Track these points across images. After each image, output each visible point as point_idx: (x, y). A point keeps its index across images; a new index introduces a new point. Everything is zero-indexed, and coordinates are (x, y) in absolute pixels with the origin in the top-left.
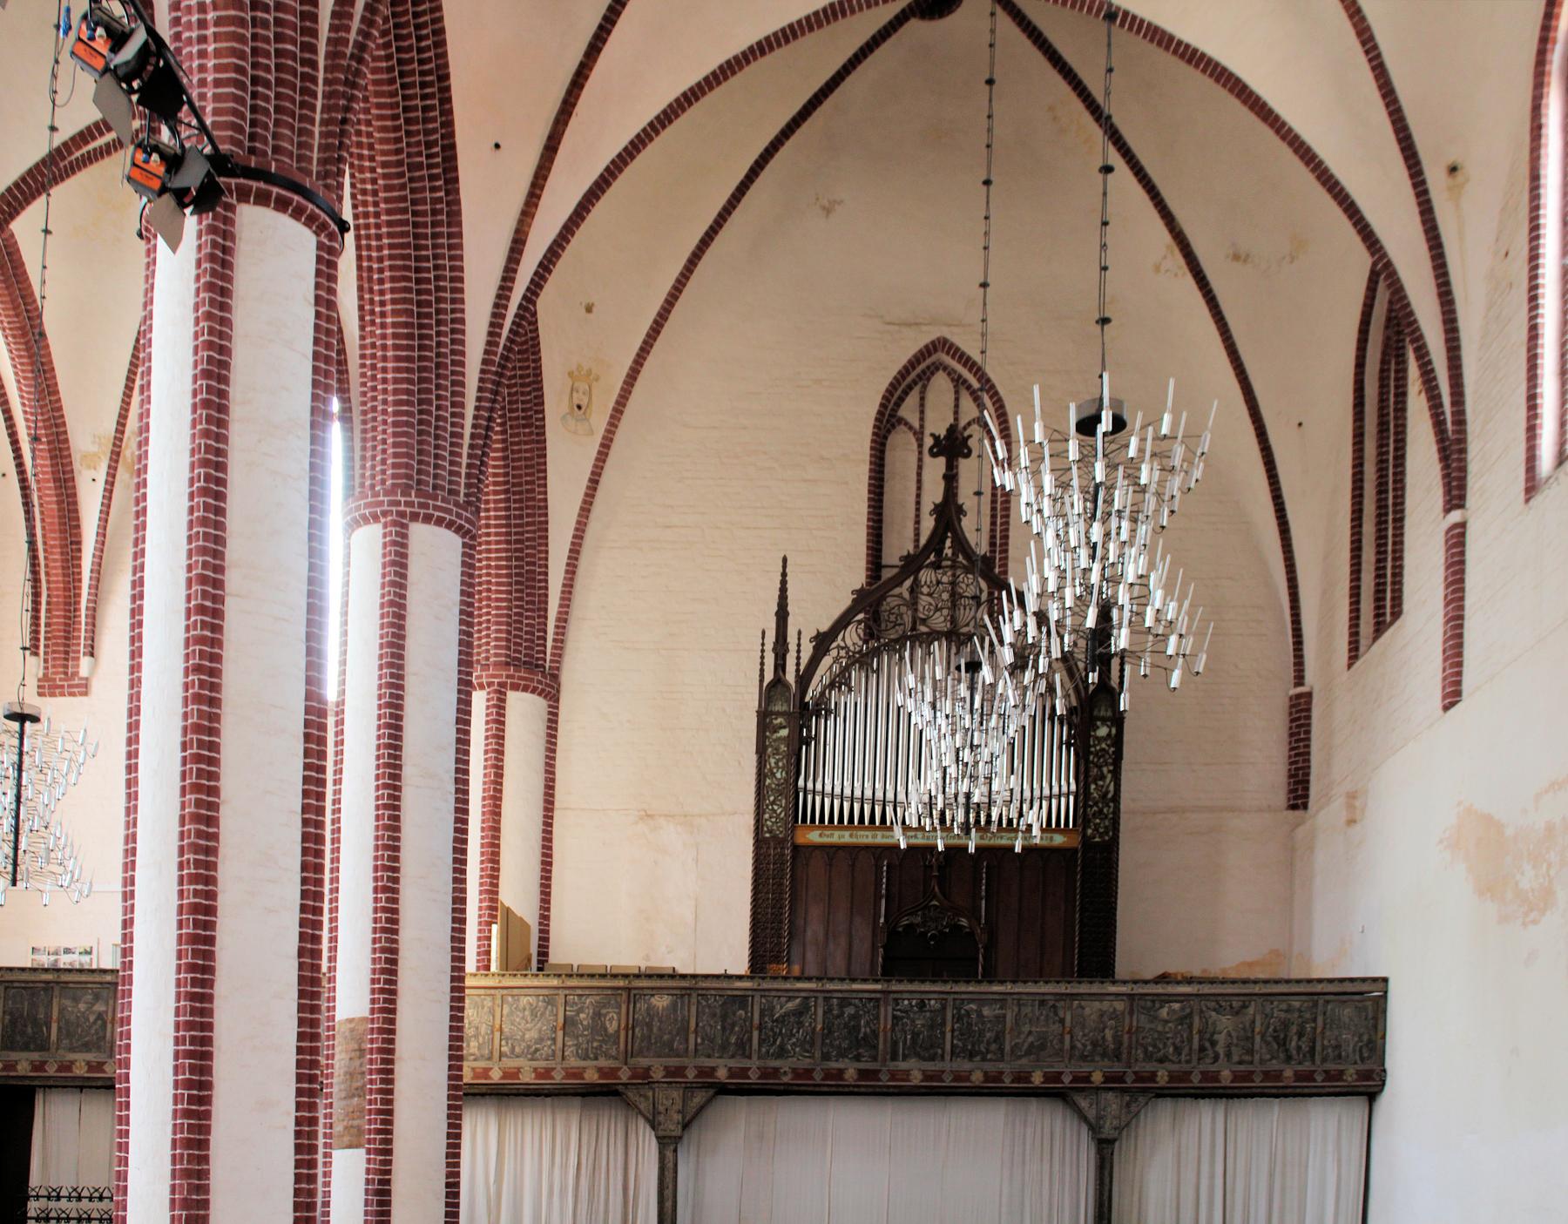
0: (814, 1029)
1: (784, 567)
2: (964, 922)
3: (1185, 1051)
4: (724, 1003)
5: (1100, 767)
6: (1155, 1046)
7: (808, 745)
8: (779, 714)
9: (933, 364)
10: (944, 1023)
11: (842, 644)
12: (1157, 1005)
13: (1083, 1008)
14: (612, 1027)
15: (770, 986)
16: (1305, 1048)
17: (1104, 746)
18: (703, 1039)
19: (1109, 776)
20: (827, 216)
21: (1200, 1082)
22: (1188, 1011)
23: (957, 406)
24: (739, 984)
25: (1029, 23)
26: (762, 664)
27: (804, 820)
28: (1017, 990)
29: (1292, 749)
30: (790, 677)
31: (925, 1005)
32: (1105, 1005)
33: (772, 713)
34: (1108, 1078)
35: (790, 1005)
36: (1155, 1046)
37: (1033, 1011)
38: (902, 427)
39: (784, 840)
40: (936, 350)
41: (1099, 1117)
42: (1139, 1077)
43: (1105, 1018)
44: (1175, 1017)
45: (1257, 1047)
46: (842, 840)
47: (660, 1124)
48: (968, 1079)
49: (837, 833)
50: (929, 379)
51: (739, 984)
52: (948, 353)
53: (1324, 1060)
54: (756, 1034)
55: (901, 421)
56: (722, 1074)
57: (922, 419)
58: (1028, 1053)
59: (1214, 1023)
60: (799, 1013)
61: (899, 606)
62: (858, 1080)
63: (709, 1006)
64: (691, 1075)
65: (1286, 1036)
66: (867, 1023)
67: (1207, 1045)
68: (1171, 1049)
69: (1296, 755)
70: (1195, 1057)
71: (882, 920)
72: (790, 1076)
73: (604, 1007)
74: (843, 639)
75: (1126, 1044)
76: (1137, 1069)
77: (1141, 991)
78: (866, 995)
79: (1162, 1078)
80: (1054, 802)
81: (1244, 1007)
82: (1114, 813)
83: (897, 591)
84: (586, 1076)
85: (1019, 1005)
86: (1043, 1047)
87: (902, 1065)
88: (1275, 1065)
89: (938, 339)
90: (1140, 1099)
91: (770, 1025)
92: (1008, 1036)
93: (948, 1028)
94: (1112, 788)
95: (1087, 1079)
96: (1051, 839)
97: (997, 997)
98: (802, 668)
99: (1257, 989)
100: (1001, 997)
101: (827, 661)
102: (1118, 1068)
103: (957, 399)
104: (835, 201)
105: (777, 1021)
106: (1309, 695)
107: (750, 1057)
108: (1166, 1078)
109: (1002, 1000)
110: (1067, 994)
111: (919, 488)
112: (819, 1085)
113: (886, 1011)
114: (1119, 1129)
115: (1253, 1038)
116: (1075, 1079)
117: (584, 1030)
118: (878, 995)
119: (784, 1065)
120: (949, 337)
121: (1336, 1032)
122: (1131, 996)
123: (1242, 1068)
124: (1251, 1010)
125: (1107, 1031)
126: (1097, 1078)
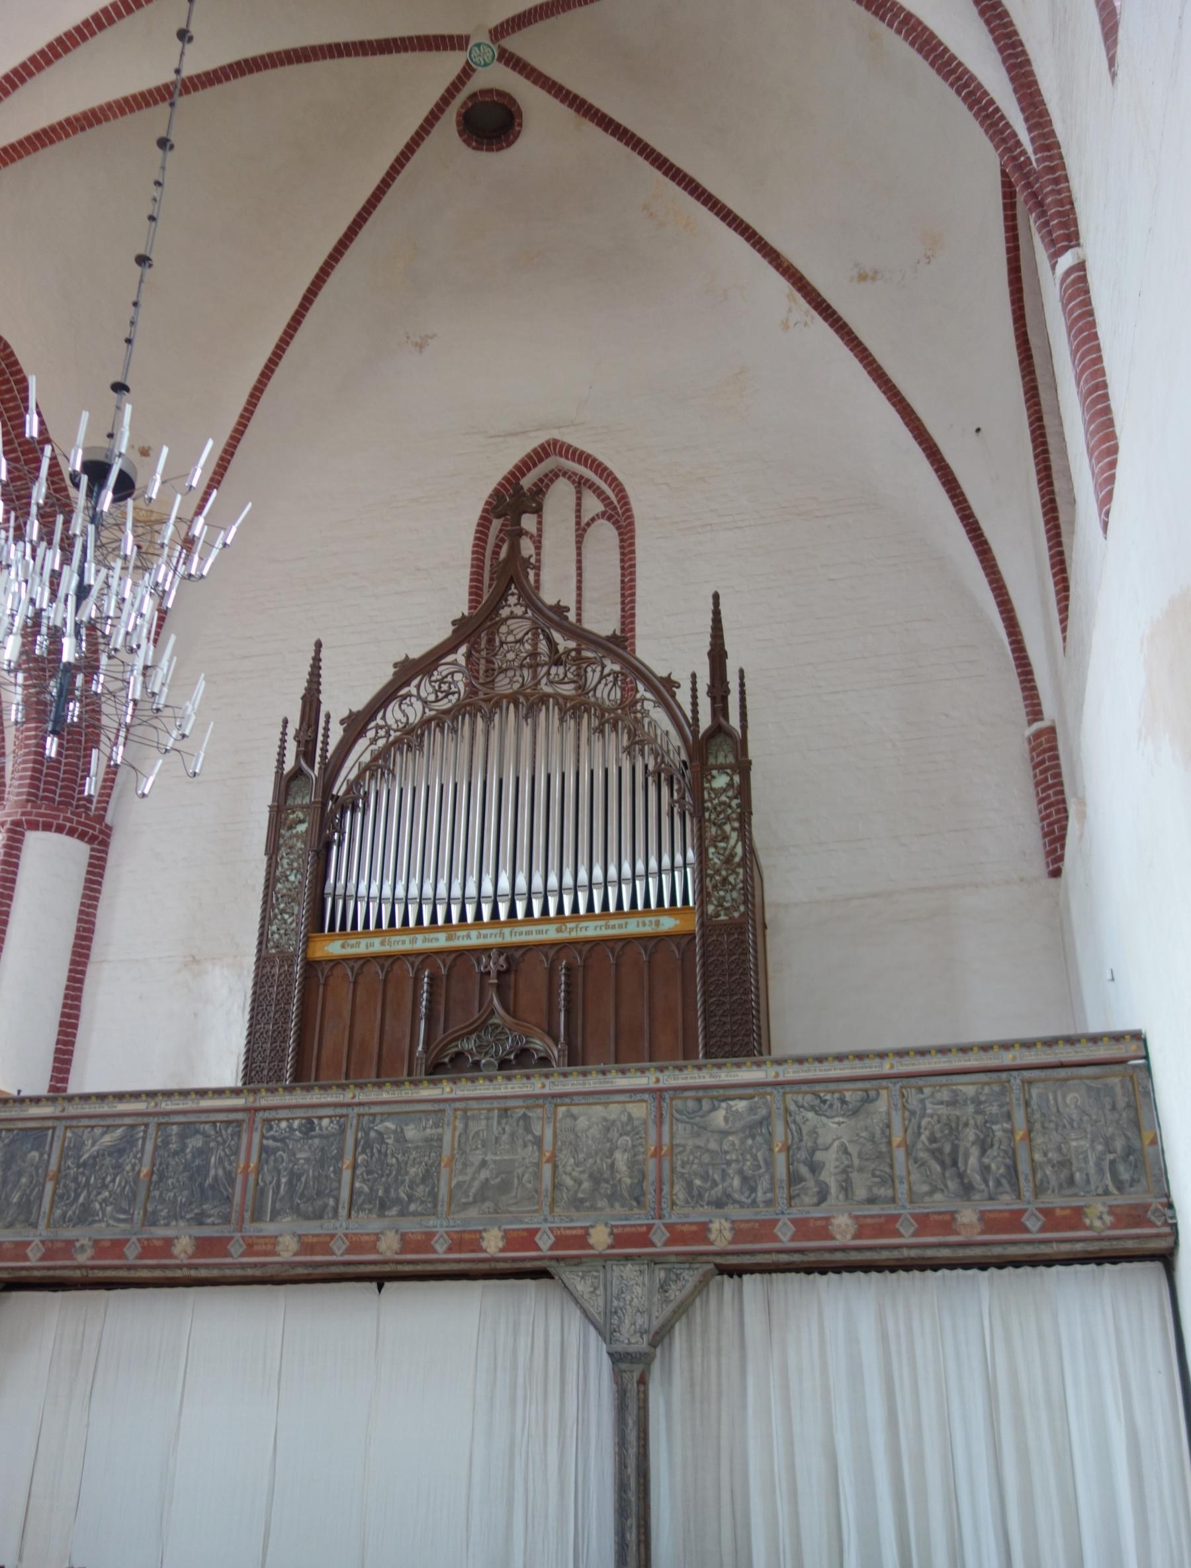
3: (763, 1184)
4: (13, 1141)
5: (720, 826)
6: (705, 1177)
10: (340, 1157)
11: (381, 723)
12: (706, 1105)
13: (575, 1118)
16: (997, 1167)
17: (723, 798)
19: (734, 835)
20: (421, 352)
21: (793, 1239)
22: (763, 1112)
24: (35, 1111)
25: (568, 92)
26: (282, 748)
28: (460, 1094)
29: (1041, 801)
31: (313, 1129)
32: (614, 1111)
34: (620, 1239)
35: (107, 1139)
36: (705, 1177)
40: (548, 455)
42: (676, 1235)
43: (614, 1134)
44: (739, 1125)
45: (900, 1170)
48: (374, 1249)
49: (363, 942)
51: (35, 1111)
53: (1038, 1190)
54: (49, 1186)
58: (481, 1197)
59: (814, 1132)
60: (118, 1151)
61: (452, 674)
65: (955, 1149)
67: (804, 1170)
68: (736, 1182)
69: (1046, 808)
70: (782, 1194)
71: (420, 1048)
72: (90, 1252)
74: (384, 718)
75: (652, 1176)
76: (674, 1219)
77: (673, 1083)
81: (867, 1100)
82: (744, 881)
85: (466, 1119)
86: (505, 1187)
87: (269, 1228)
88: (939, 1203)
89: (548, 442)
90: (686, 1274)
91: (72, 1172)
92: (444, 1172)
93: (348, 1161)
94: (739, 850)
95: (582, 1240)
96: (658, 923)
99: (886, 1067)
100: (437, 1107)
101: (362, 743)
102: (638, 1219)
103: (579, 499)
104: (427, 336)
105: (84, 1164)
106: (1052, 730)
107: (35, 1225)
108: (728, 1235)
109: (437, 1110)
110: (545, 1096)
115: (890, 1152)
118: (239, 1116)
120: (558, 437)
121: (1056, 1137)
122: (658, 1093)
123: (875, 1210)
124: (882, 1105)
126: (600, 1238)
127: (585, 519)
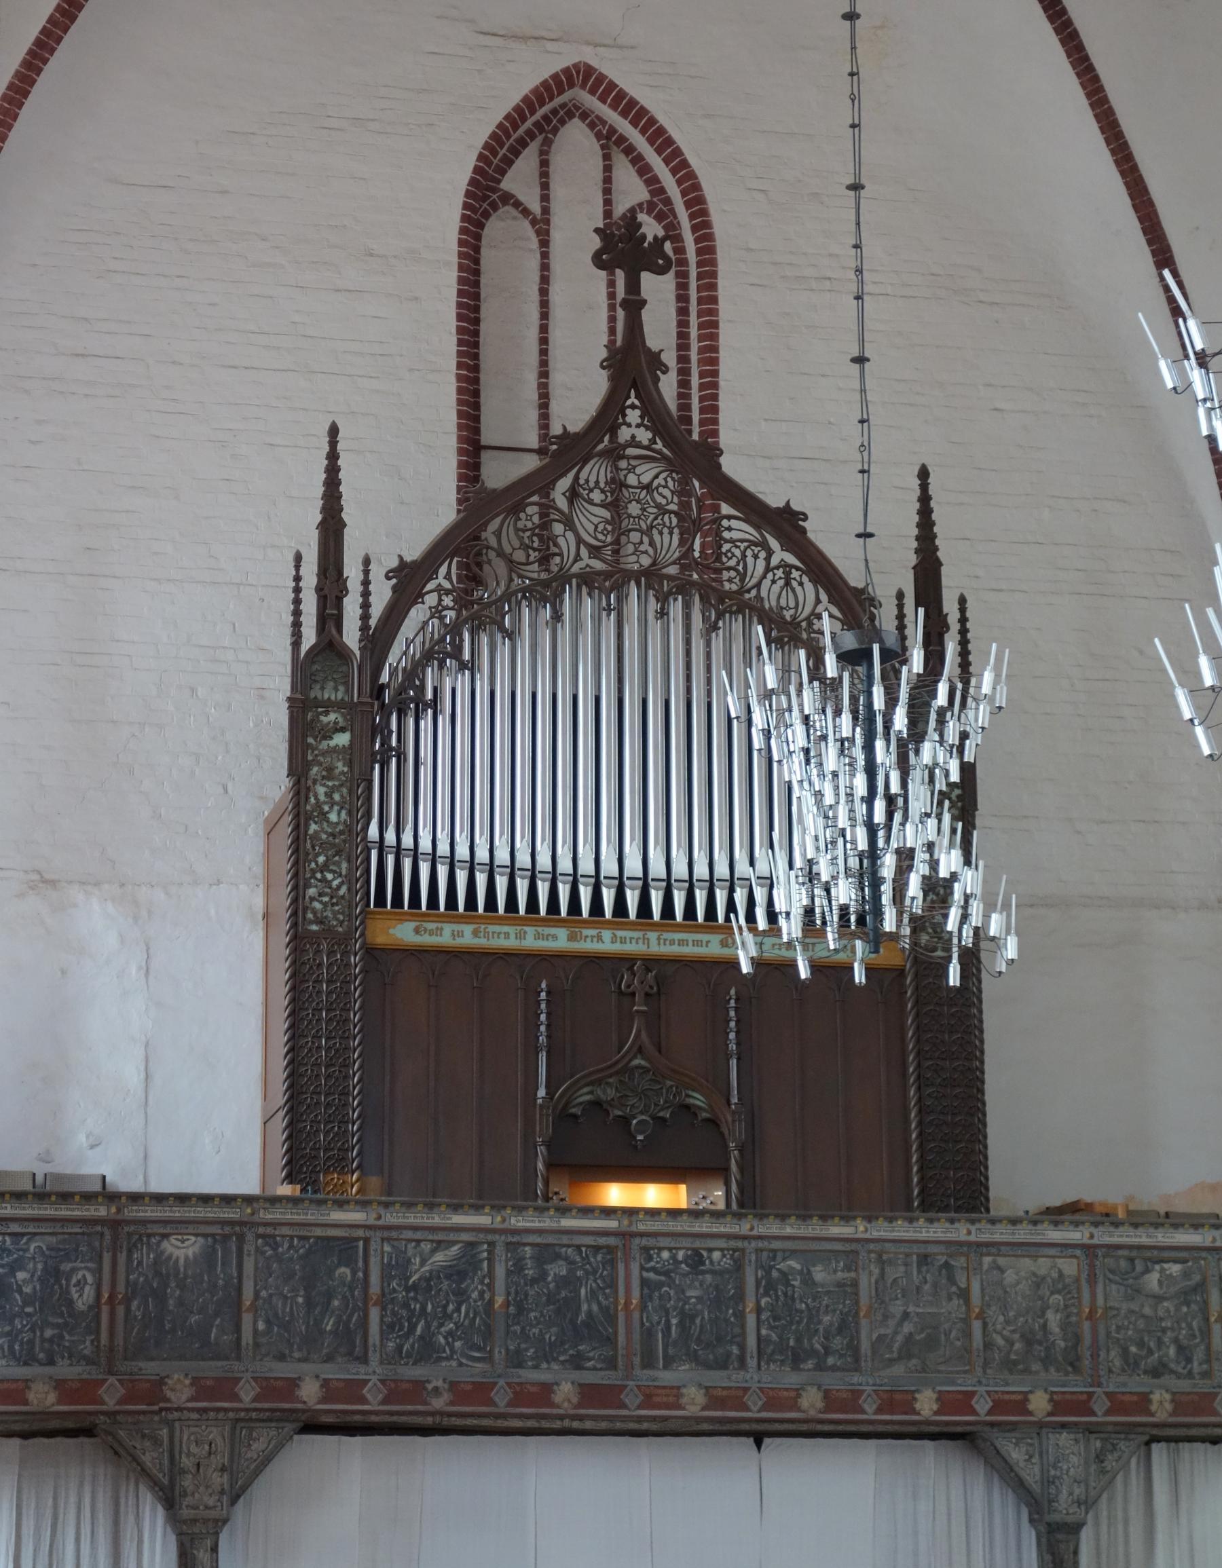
0: (491, 1302)
1: (333, 443)
2: (698, 1099)
3: (1199, 1354)
6: (1141, 1344)
7: (384, 765)
8: (329, 706)
9: (563, 106)
10: (740, 1297)
12: (1139, 1267)
13: (1001, 1270)
14: (83, 1299)
15: (400, 1221)
18: (268, 1322)
22: (1197, 1278)
23: (607, 180)
26: (297, 613)
27: (381, 900)
28: (875, 1234)
30: (351, 636)
32: (1042, 1266)
33: (317, 703)
34: (1060, 1405)
35: (440, 1258)
37: (908, 1274)
38: (509, 209)
39: (347, 938)
40: (571, 85)
41: (1048, 1482)
42: (1117, 1405)
44: (1173, 1290)
46: (460, 942)
47: (184, 1494)
48: (795, 1407)
49: (448, 928)
50: (555, 131)
52: (592, 92)
55: (508, 198)
56: (309, 1392)
57: (545, 198)
58: (907, 1351)
60: (459, 1273)
62: (579, 1405)
63: (279, 1258)
64: (247, 1394)
66: (593, 1294)
68: (1172, 1351)
71: (542, 1093)
73: (67, 1257)
76: (1111, 1389)
77: (1107, 1240)
78: (589, 1240)
79: (1161, 1404)
84: (31, 1396)
85: (881, 1261)
86: (932, 1343)
87: (666, 1377)
90: (1122, 1445)
91: (401, 1295)
92: (864, 1322)
93: (750, 1305)
95: (1021, 1406)
97: (838, 1246)
98: (373, 622)
101: (417, 615)
102: (1076, 1386)
103: (608, 169)
105: (415, 1287)
107: (364, 1360)
108: (1169, 1406)
109: (850, 1253)
110: (969, 1244)
111: (545, 316)
112: (504, 1416)
113: (627, 1268)
114: (1088, 1503)
116: (998, 1406)
117: (26, 1303)
119: (435, 1375)
120: (594, 63)
122: (1089, 1250)
125: (1050, 1315)
126: (1039, 1403)
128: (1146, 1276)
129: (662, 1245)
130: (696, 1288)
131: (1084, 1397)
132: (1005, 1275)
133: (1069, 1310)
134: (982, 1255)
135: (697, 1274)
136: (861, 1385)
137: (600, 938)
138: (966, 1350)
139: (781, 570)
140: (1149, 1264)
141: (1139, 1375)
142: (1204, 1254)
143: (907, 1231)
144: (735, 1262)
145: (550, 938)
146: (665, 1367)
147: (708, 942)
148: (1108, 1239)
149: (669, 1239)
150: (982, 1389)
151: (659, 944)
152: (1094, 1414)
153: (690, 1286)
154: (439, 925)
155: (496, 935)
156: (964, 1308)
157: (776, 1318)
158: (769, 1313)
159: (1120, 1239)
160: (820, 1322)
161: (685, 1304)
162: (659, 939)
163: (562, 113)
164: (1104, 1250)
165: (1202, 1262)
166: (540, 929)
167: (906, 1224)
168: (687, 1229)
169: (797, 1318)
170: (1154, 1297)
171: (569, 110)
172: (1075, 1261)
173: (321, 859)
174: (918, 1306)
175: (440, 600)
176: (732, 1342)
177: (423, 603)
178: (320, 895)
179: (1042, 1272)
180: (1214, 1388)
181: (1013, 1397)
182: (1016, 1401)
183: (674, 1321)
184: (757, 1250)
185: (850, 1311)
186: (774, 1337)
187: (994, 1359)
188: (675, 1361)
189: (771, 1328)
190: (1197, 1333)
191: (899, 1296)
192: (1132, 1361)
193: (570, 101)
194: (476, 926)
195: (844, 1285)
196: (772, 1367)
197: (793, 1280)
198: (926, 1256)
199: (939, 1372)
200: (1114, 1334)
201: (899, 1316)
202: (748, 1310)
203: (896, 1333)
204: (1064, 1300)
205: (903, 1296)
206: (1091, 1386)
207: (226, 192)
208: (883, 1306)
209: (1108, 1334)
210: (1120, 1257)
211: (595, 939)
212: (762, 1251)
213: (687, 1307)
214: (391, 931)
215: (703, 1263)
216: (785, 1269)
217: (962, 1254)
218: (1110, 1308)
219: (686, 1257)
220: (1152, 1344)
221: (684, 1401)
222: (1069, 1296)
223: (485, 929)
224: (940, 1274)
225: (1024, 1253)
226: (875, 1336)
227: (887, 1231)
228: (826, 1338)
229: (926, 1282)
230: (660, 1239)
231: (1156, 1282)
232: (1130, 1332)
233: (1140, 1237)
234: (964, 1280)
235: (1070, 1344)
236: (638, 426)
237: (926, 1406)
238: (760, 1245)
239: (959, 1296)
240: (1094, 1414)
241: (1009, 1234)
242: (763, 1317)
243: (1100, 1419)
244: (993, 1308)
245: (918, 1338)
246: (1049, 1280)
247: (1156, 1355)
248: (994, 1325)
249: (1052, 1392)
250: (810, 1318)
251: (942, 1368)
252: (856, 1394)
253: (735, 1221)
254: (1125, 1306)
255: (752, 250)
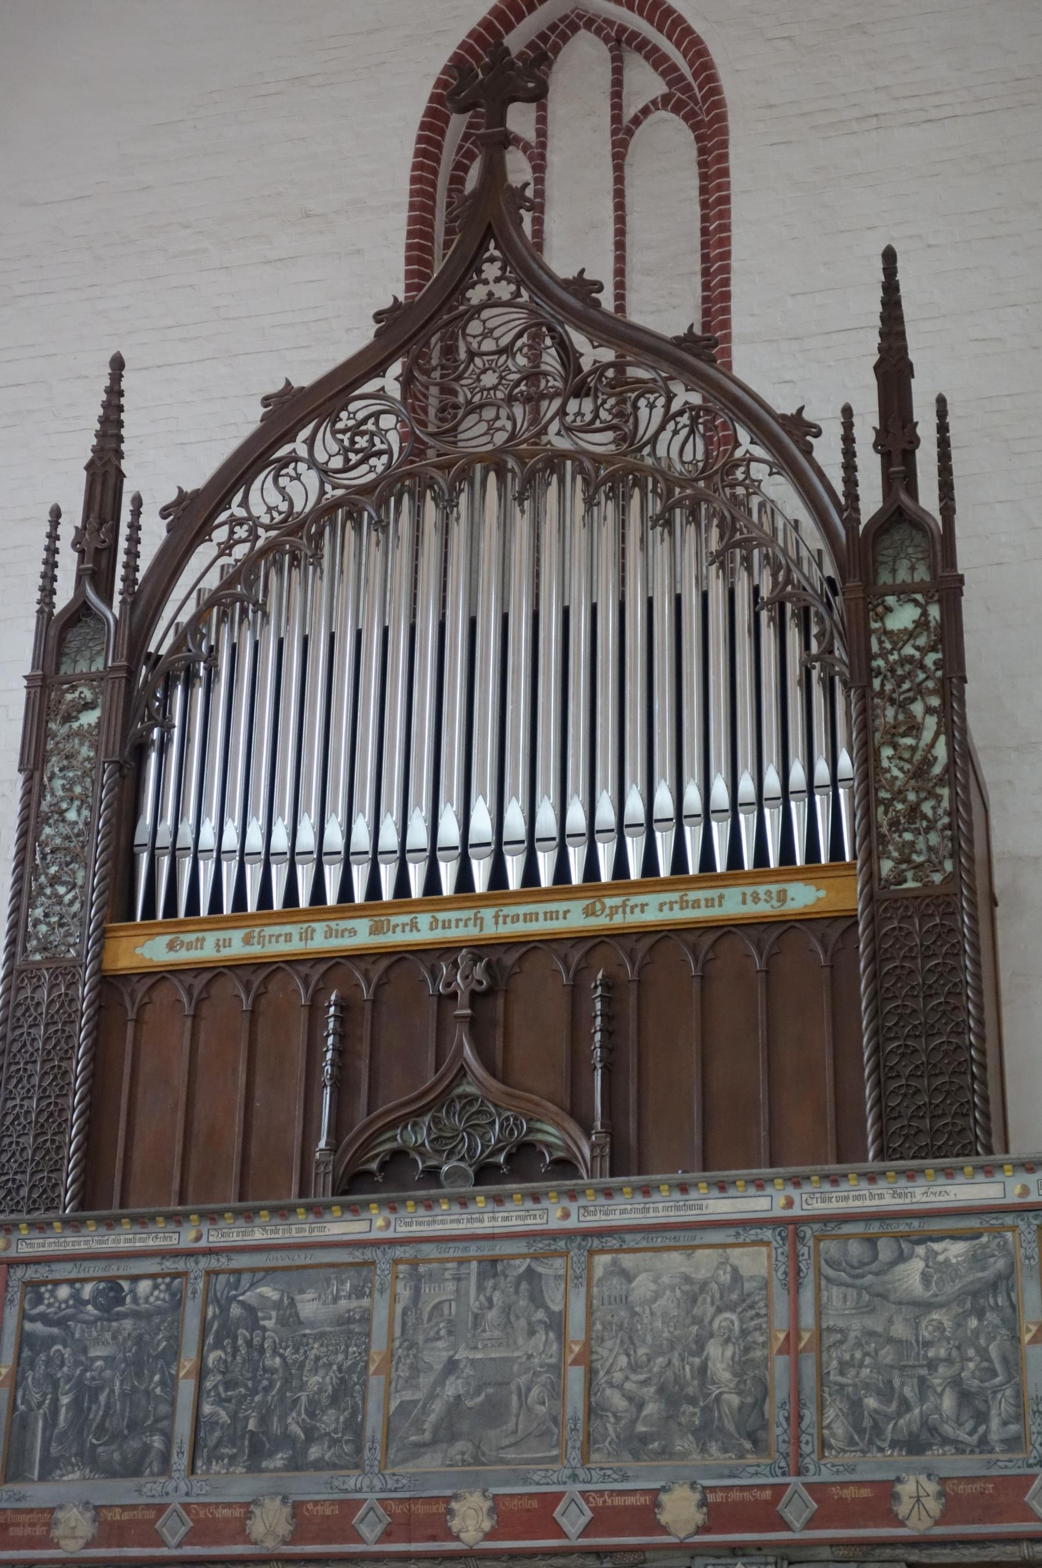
3: (1001, 1407)
5: (902, 706)
6: (886, 1393)
10: (173, 1354)
11: (241, 513)
12: (886, 1250)
13: (628, 1276)
17: (909, 650)
19: (931, 723)
22: (1001, 1264)
26: (51, 564)
28: (402, 1230)
43: (705, 1308)
44: (952, 1289)
46: (226, 953)
48: (242, 1535)
49: (211, 938)
61: (377, 415)
68: (948, 1403)
76: (826, 1476)
77: (819, 1207)
80: (798, 810)
83: (371, 386)
85: (417, 1280)
92: (376, 1383)
93: (188, 1362)
94: (941, 751)
96: (782, 897)
103: (618, 71)
108: (934, 1507)
110: (569, 1235)
125: (713, 1349)
127: (630, 111)
128: (901, 1267)
129: (57, 1276)
130: (105, 1343)
131: (767, 1494)
132: (634, 1284)
133: (749, 1339)
134: (591, 1253)
135: (109, 1320)
136: (360, 1490)
137: (414, 926)
138: (555, 1421)
139: (686, 415)
140: (905, 1246)
141: (881, 1450)
142: (1009, 1220)
143: (459, 1221)
144: (173, 1295)
145: (346, 934)
146: (42, 1478)
147: (566, 912)
148: (820, 1205)
149: (69, 1266)
150: (573, 1489)
151: (497, 923)
152: (786, 1527)
153: (97, 1341)
154: (200, 935)
155: (274, 939)
156: (555, 1347)
157: (229, 1385)
158: (219, 1377)
159: (857, 1203)
160: (302, 1387)
161: (85, 1370)
162: (496, 917)
163: (562, 26)
164: (816, 1227)
165: (1009, 1235)
166: (333, 924)
167: (456, 1209)
168: (96, 1247)
169: (265, 1383)
170: (915, 1303)
171: (572, 22)
172: (764, 1250)
173: (53, 870)
174: (475, 1348)
175: (232, 532)
176: (152, 1430)
177: (211, 540)
178: (46, 915)
179: (702, 1274)
180: (1030, 1466)
181: (630, 1500)
182: (633, 1508)
183: (65, 1400)
184: (208, 1273)
185: (355, 1364)
186: (224, 1417)
187: (605, 1436)
188: (58, 1467)
189: (220, 1401)
190: (998, 1367)
191: (443, 1333)
192: (867, 1423)
193: (572, 12)
194: (247, 930)
195: (350, 1320)
196: (215, 1467)
197: (264, 1318)
198: (494, 1261)
199: (503, 1461)
200: (834, 1377)
201: (438, 1367)
202: (182, 1373)
203: (432, 1397)
204: (742, 1322)
205: (450, 1333)
206: (784, 1474)
207: (148, 187)
208: (414, 1351)
209: (822, 1378)
210: (848, 1237)
211: (408, 928)
212: (217, 1273)
213: (88, 1374)
214: (138, 951)
215: (121, 1301)
216: (253, 1302)
217: (556, 1254)
218: (828, 1329)
219: (97, 1294)
220: (907, 1391)
221: (57, 1532)
222: (752, 1313)
223: (260, 933)
224: (517, 1291)
225: (667, 1243)
226: (394, 1405)
227: (421, 1224)
228: (311, 1414)
229: (491, 1305)
230: (55, 1266)
231: (917, 1277)
232: (865, 1372)
233: (881, 1196)
234: (559, 1296)
235: (749, 1400)
236: (497, 280)
237: (471, 1524)
238: (213, 1263)
239: (548, 1327)
240: (786, 1527)
241: (636, 1210)
242: (208, 1384)
243: (797, 1536)
244: (609, 1344)
245: (469, 1403)
246: (714, 1287)
247: (917, 1411)
248: (608, 1372)
249: (704, 1488)
250: (287, 1381)
251: (510, 1455)
252: (349, 1507)
253: (172, 1227)
254: (855, 1326)
255: (774, 106)
